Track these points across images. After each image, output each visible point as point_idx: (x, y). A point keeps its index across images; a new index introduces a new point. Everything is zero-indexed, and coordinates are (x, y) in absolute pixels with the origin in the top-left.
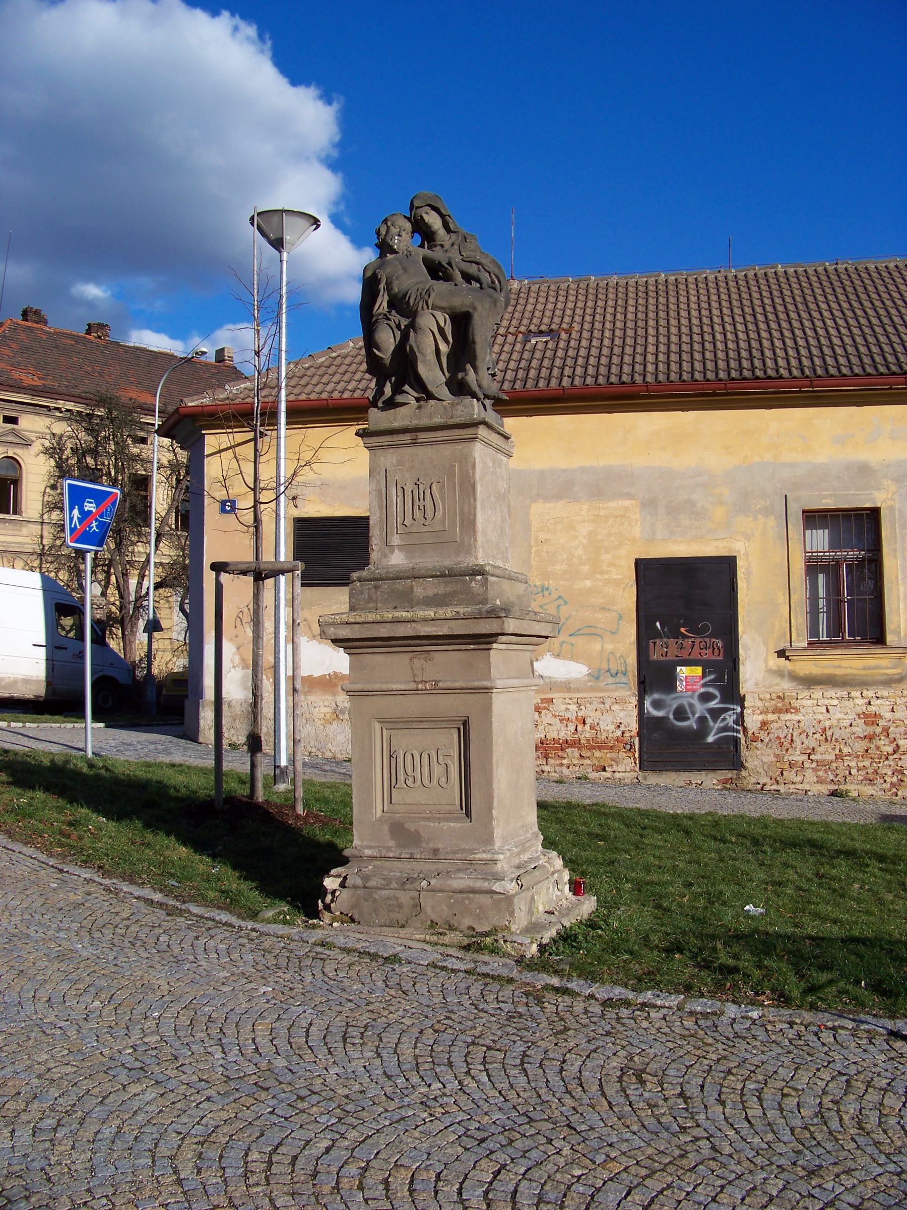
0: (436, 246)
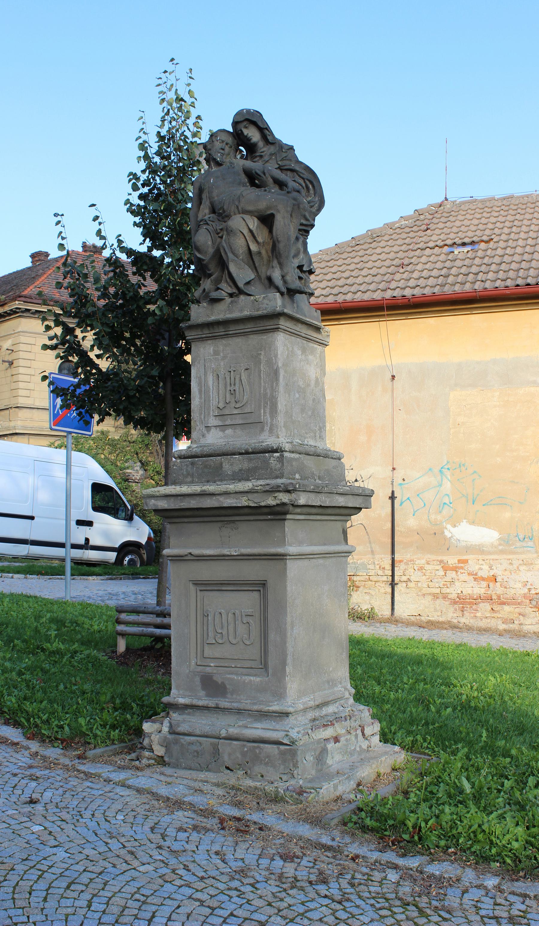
0: (256, 157)
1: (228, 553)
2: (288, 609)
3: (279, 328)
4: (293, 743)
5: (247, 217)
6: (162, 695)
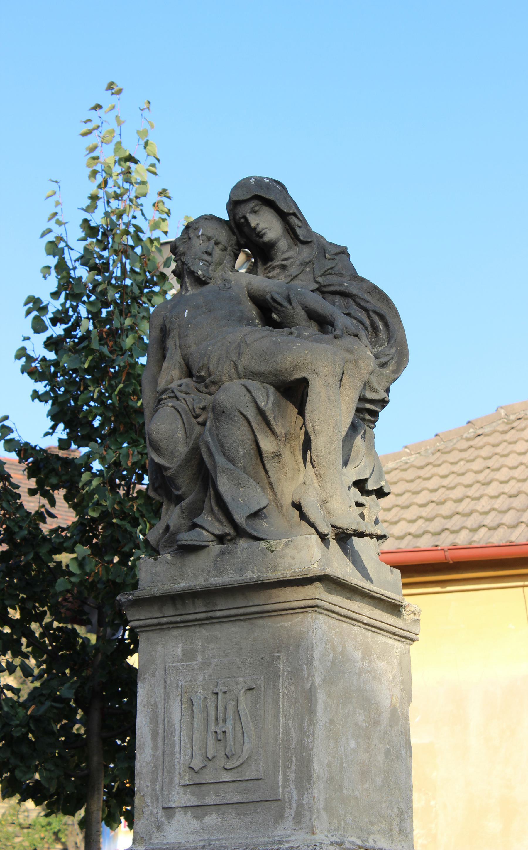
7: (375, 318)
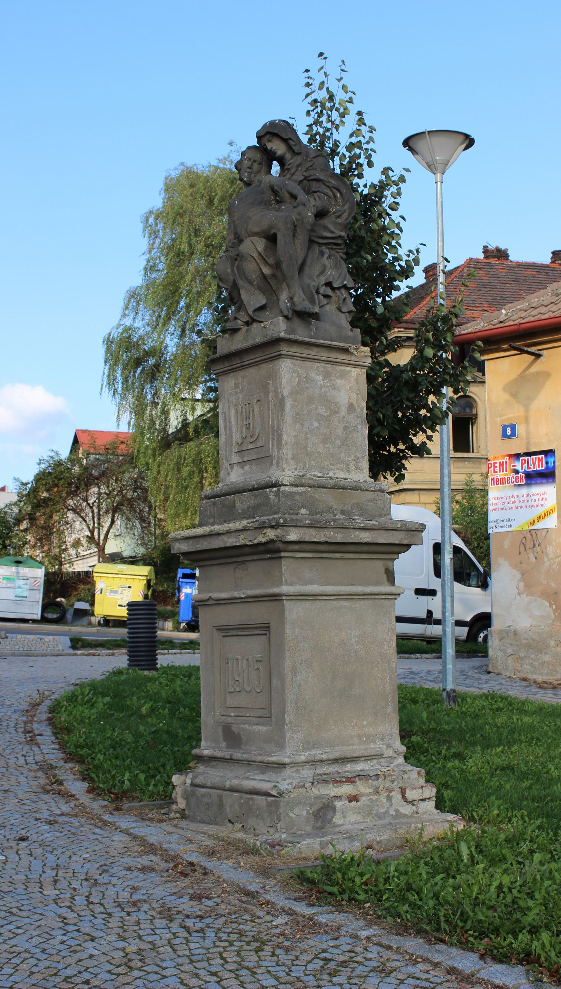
1: (238, 596)
2: (288, 654)
3: (281, 355)
4: (281, 795)
5: (254, 239)
6: (193, 747)
7: (335, 191)
